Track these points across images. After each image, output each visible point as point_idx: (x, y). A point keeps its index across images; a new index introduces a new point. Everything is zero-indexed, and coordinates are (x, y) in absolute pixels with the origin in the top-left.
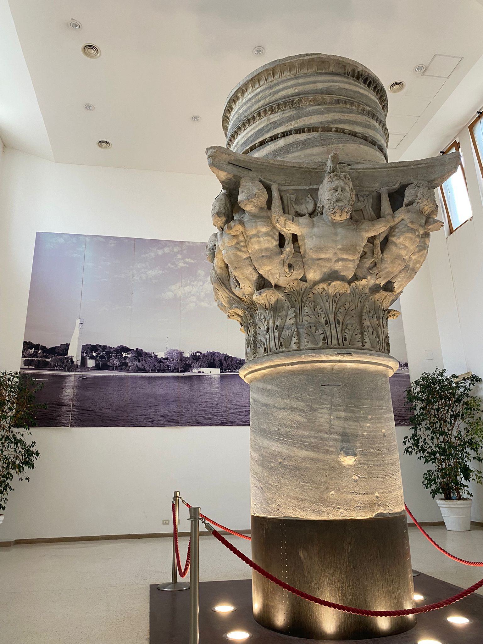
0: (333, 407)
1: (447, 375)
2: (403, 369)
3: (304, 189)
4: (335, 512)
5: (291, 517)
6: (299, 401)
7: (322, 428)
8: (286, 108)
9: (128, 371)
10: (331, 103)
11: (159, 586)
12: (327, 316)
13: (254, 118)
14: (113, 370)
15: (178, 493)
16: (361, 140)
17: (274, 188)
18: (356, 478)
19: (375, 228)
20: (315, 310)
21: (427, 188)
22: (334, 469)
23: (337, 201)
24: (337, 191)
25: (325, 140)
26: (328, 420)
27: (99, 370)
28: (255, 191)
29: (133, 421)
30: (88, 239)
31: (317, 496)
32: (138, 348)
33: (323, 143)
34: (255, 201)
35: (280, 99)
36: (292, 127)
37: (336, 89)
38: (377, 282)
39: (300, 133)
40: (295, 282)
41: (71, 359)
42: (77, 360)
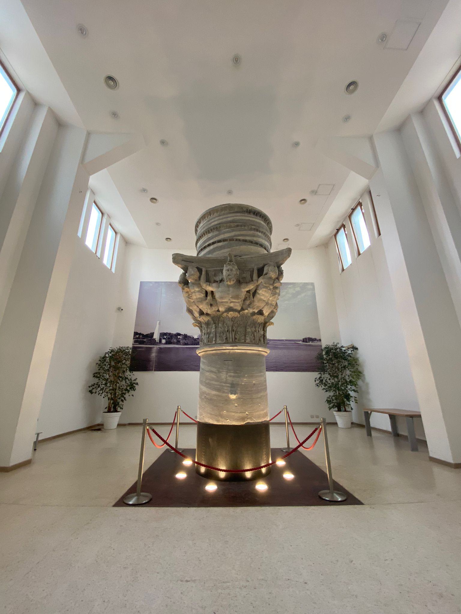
1: (339, 346)
9: (180, 345)
10: (234, 227)
13: (202, 235)
19: (248, 287)
22: (226, 400)
26: (225, 377)
28: (193, 273)
35: (212, 226)
38: (254, 311)
40: (214, 312)
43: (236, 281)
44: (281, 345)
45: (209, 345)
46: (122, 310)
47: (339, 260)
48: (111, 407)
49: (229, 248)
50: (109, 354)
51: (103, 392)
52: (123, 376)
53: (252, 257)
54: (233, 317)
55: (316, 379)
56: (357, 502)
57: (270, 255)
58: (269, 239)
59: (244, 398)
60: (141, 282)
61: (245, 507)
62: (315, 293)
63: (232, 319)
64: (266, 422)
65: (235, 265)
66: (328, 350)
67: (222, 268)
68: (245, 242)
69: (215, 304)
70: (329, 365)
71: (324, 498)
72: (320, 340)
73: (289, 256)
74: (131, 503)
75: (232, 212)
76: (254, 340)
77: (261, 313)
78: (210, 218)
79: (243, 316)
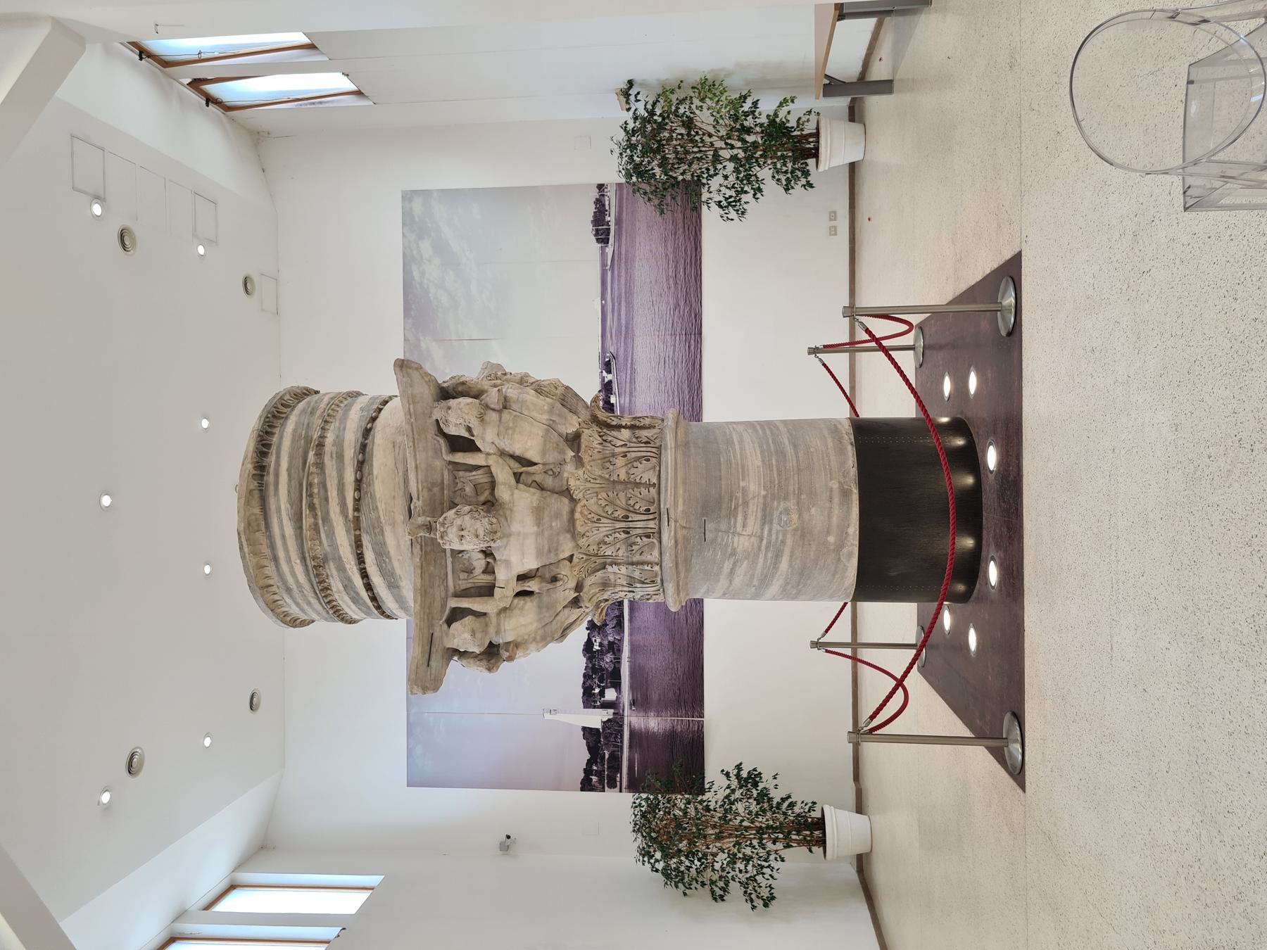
1: (621, 135)
3: (452, 563)
7: (756, 545)
9: (621, 640)
10: (315, 516)
11: (918, 366)
14: (619, 663)
16: (366, 468)
17: (454, 603)
21: (450, 412)
23: (477, 536)
24: (462, 536)
25: (374, 528)
27: (620, 683)
29: (695, 631)
32: (586, 628)
33: (378, 530)
35: (310, 581)
36: (355, 568)
37: (292, 508)
39: (363, 557)
41: (604, 722)
42: (607, 714)
44: (619, 315)
46: (508, 837)
47: (321, 103)
50: (657, 861)
51: (769, 866)
53: (414, 465)
56: (1016, 260)
59: (796, 492)
63: (595, 519)
65: (445, 519)
76: (648, 460)
78: (278, 588)
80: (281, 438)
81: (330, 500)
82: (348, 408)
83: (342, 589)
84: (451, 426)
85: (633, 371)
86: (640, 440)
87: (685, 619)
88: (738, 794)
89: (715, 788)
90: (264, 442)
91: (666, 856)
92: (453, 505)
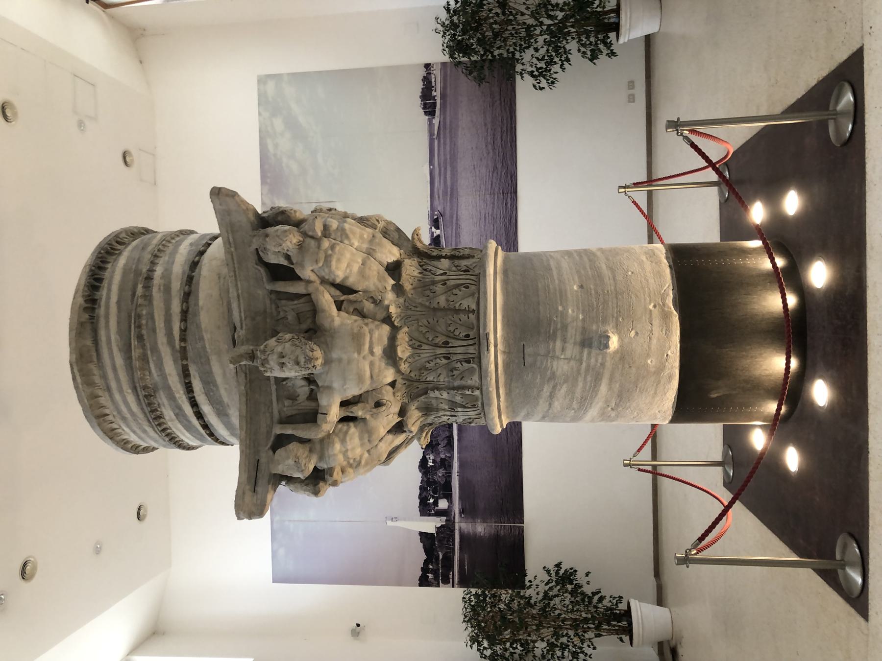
0: (550, 354)
1: (444, 16)
2: (434, 72)
3: (276, 389)
4: (671, 360)
5: (674, 402)
6: (543, 390)
7: (575, 369)
8: (156, 402)
9: (452, 457)
10: (143, 347)
11: (723, 201)
12: (438, 356)
15: (626, 462)
16: (192, 300)
17: (278, 430)
18: (633, 334)
20: (431, 369)
21: (267, 239)
22: (622, 358)
23: (298, 363)
24: (283, 363)
26: (566, 361)
27: (451, 494)
28: (291, 462)
30: (277, 518)
31: (653, 379)
33: (204, 361)
34: (304, 462)
35: (142, 409)
38: (389, 288)
39: (191, 386)
40: (397, 394)
41: (438, 528)
42: (439, 521)
43: (311, 341)
44: (445, 177)
45: (483, 404)
46: (358, 625)
48: (617, 628)
49: (208, 361)
50: (485, 648)
52: (539, 605)
53: (236, 294)
54: (410, 346)
55: (537, 85)
57: (231, 246)
58: (169, 238)
59: (615, 315)
60: (275, 581)
61: (868, 324)
62: (288, 74)
64: (669, 255)
65: (266, 347)
66: (456, 47)
67: (272, 381)
68: (190, 316)
69: (374, 393)
70: (499, 48)
71: (848, 135)
72: (427, 66)
73: (233, 195)
74: (859, 580)
75: (95, 354)
76: (467, 287)
77: (394, 269)
78: (114, 416)
79: (406, 319)
80: (113, 272)
81: (158, 331)
82: (179, 244)
83: (175, 417)
84: (269, 254)
85: (458, 226)
86: (459, 268)
87: (506, 439)
88: (555, 591)
89: (537, 582)
90: (96, 276)
91: (492, 644)
92: (275, 333)
